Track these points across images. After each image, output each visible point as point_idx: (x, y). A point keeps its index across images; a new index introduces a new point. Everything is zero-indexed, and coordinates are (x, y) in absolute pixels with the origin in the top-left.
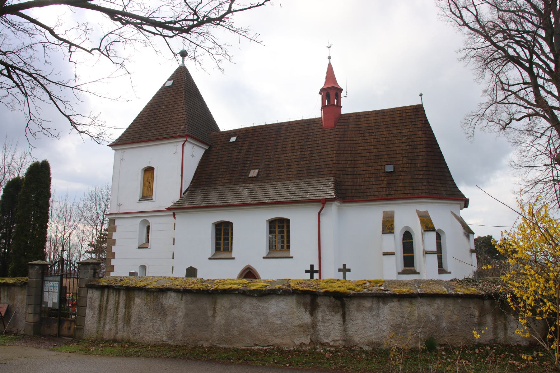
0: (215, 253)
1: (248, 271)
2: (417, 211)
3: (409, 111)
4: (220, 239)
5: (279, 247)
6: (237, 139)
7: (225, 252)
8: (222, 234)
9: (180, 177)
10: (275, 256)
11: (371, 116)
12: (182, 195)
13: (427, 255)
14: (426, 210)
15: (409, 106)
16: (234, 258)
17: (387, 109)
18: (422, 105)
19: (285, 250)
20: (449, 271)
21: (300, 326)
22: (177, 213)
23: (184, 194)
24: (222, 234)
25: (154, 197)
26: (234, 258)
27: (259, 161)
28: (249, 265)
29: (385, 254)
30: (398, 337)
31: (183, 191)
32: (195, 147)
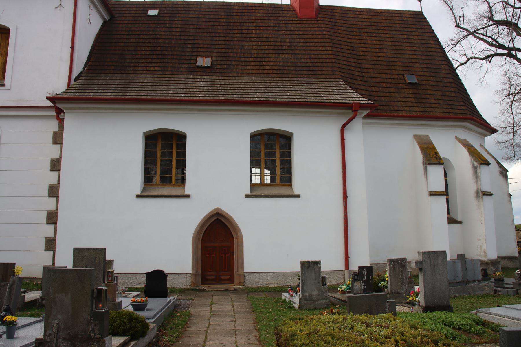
0: (144, 187)
1: (215, 218)
2: (415, 136)
3: (340, 12)
4: (155, 163)
5: (156, 179)
6: (159, 11)
7: (165, 185)
8: (278, 155)
9: (69, 50)
10: (156, 193)
11: (362, 13)
12: (73, 82)
13: (485, 197)
14: (465, 138)
15: (407, 11)
16: (188, 197)
17: (380, 10)
18: (422, 11)
19: (278, 185)
20: (459, 220)
21: (452, 311)
22: (67, 109)
23: (76, 80)
24: (278, 155)
25: (7, 81)
26: (188, 197)
27: (208, 46)
28: (218, 209)
29: (490, 194)
30: (426, 327)
31: (75, 74)
32: (92, 7)
